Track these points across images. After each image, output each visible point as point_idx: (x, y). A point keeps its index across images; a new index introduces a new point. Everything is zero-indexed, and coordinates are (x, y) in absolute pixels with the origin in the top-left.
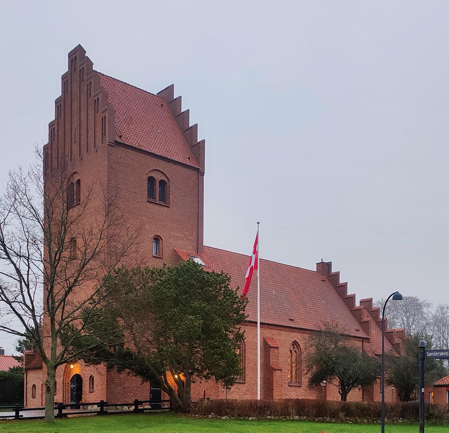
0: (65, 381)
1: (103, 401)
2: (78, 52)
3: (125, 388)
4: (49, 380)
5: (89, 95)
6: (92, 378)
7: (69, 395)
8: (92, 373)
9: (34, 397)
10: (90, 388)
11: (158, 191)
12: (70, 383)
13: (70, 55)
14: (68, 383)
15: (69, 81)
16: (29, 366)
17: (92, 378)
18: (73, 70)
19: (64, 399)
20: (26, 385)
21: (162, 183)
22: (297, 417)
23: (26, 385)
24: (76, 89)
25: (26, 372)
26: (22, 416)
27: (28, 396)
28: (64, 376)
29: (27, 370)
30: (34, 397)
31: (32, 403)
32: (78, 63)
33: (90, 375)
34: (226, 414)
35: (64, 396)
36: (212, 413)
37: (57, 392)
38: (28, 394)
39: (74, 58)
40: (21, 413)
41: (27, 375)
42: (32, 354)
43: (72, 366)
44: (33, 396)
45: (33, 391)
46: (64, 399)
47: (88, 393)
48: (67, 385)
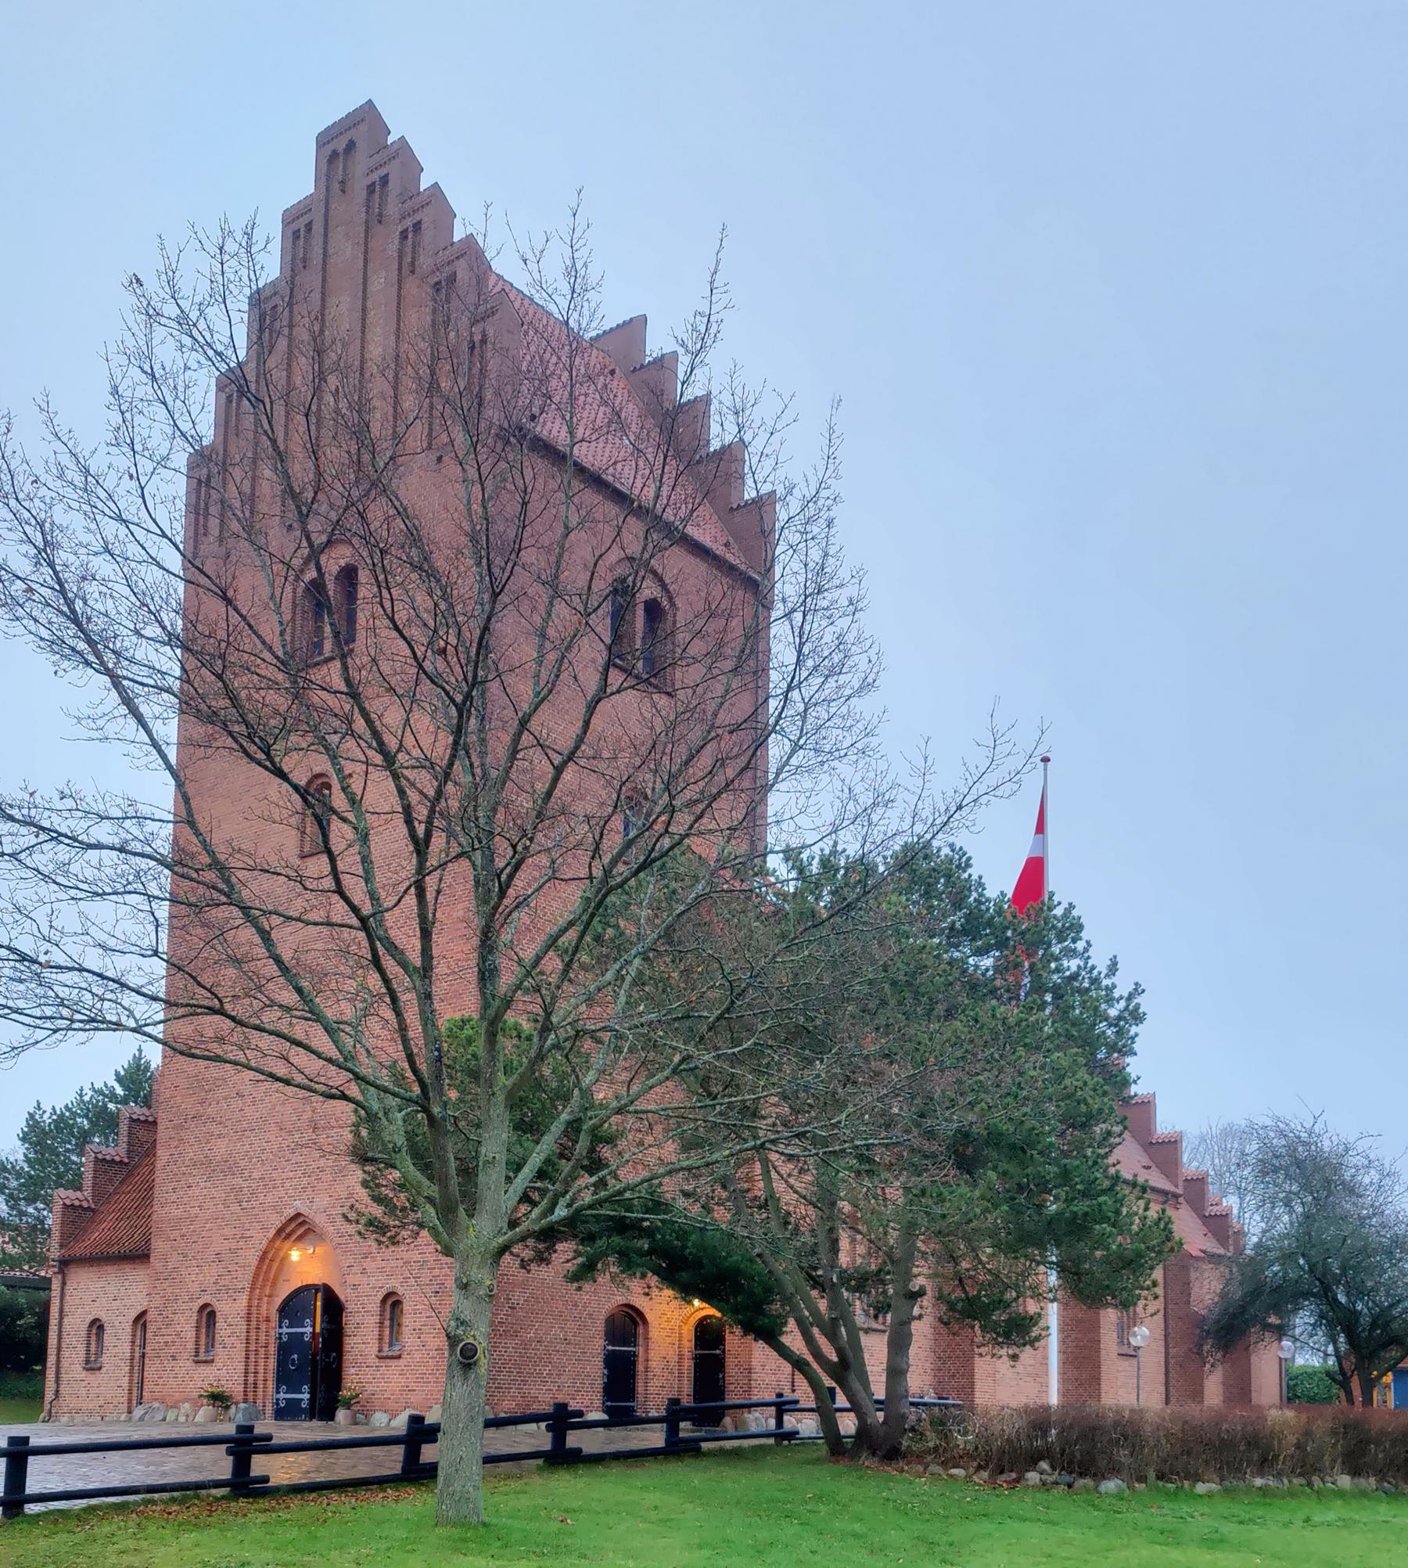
0: (254, 1310)
1: (565, 1405)
2: (363, 127)
3: (525, 1344)
4: (467, 1315)
5: (406, 270)
6: (392, 1304)
7: (272, 1363)
8: (393, 1284)
9: (92, 1365)
10: (381, 1339)
11: (640, 637)
12: (275, 1317)
13: (324, 140)
14: (268, 1320)
15: (318, 228)
16: (79, 1249)
17: (392, 1304)
18: (336, 186)
19: (251, 1379)
20: (61, 1318)
21: (653, 610)
22: (1345, 1481)
23: (61, 1318)
24: (345, 250)
25: (62, 1272)
26: (266, 1479)
27: (65, 1364)
28: (252, 1289)
29: (65, 1264)
30: (92, 1365)
31: (83, 1391)
32: (361, 161)
33: (384, 1292)
34: (1114, 1470)
35: (252, 1369)
36: (1044, 1465)
37: (219, 1349)
38: (65, 1353)
39: (340, 150)
40: (260, 1465)
41: (64, 1284)
42: (85, 1205)
43: (295, 1255)
44: (87, 1362)
45: (89, 1344)
46: (251, 1379)
47: (372, 1359)
48: (263, 1326)
